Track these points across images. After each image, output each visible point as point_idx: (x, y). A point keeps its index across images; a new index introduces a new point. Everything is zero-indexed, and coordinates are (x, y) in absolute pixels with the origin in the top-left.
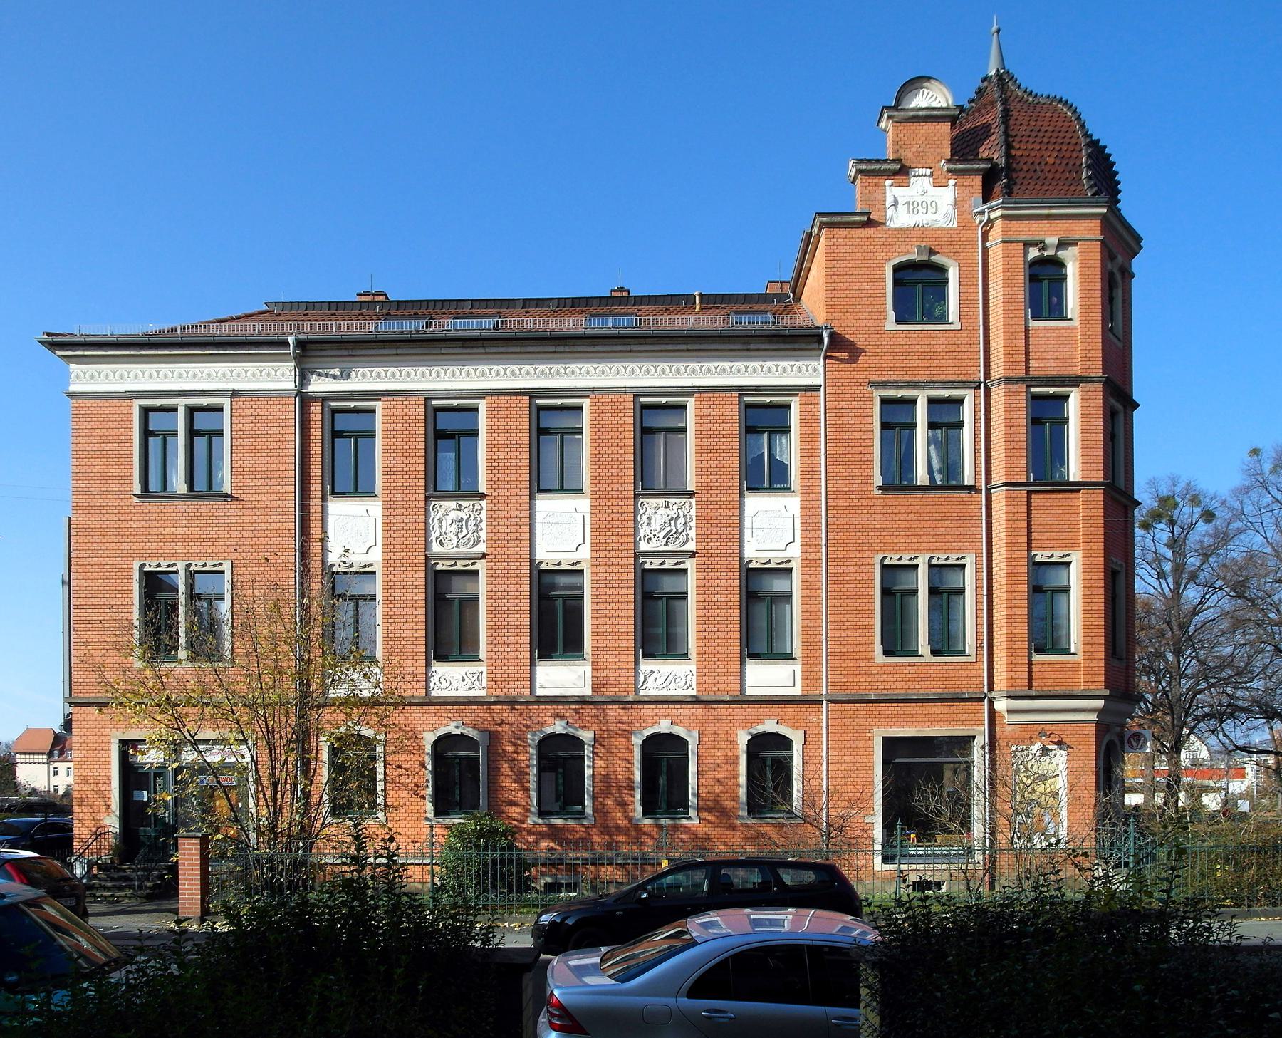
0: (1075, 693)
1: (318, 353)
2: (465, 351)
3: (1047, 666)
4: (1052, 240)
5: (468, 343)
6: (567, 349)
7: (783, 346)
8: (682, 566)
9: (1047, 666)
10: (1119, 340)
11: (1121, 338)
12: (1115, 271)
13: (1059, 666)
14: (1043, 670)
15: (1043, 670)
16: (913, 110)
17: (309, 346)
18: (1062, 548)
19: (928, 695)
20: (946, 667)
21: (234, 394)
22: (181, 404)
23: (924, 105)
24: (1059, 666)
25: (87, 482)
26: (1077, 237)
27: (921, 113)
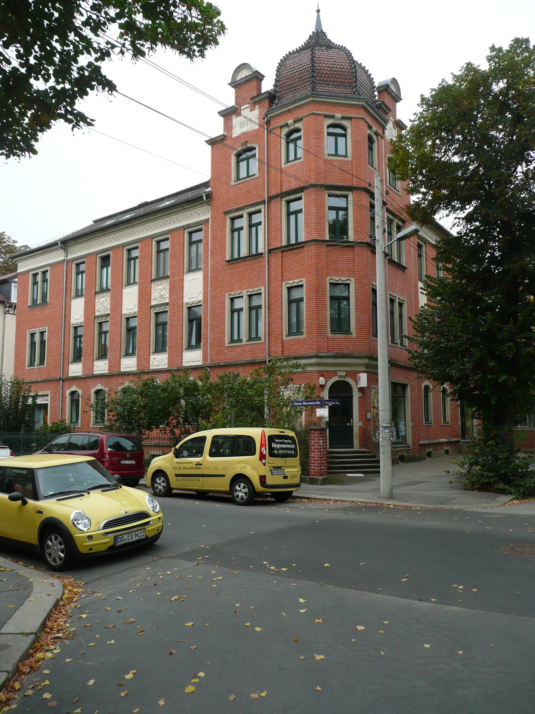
0: (299, 356)
1: (69, 244)
2: (105, 233)
3: (291, 342)
4: (290, 121)
5: (105, 230)
6: (130, 225)
7: (194, 204)
8: (165, 310)
9: (291, 342)
10: (376, 170)
11: (377, 169)
12: (372, 134)
13: (296, 341)
14: (290, 344)
15: (290, 344)
16: (239, 80)
17: (66, 243)
18: (298, 278)
19: (243, 361)
20: (253, 346)
21: (50, 265)
22: (39, 271)
23: (244, 76)
24: (296, 341)
25: (339, 342)
26: (301, 116)
27: (243, 81)
